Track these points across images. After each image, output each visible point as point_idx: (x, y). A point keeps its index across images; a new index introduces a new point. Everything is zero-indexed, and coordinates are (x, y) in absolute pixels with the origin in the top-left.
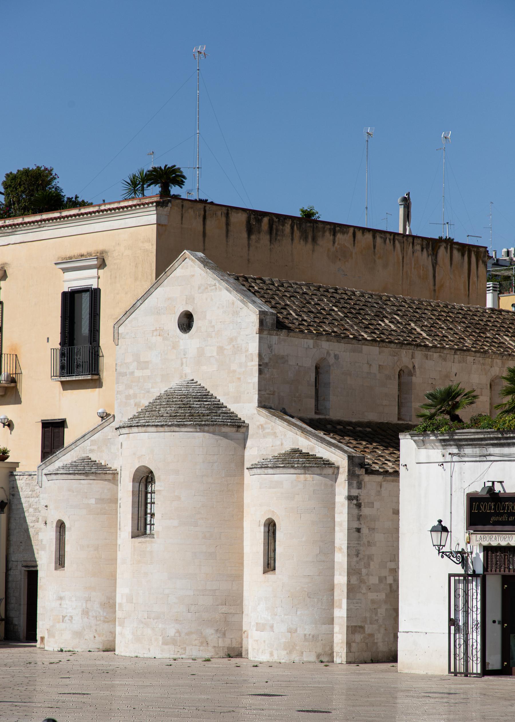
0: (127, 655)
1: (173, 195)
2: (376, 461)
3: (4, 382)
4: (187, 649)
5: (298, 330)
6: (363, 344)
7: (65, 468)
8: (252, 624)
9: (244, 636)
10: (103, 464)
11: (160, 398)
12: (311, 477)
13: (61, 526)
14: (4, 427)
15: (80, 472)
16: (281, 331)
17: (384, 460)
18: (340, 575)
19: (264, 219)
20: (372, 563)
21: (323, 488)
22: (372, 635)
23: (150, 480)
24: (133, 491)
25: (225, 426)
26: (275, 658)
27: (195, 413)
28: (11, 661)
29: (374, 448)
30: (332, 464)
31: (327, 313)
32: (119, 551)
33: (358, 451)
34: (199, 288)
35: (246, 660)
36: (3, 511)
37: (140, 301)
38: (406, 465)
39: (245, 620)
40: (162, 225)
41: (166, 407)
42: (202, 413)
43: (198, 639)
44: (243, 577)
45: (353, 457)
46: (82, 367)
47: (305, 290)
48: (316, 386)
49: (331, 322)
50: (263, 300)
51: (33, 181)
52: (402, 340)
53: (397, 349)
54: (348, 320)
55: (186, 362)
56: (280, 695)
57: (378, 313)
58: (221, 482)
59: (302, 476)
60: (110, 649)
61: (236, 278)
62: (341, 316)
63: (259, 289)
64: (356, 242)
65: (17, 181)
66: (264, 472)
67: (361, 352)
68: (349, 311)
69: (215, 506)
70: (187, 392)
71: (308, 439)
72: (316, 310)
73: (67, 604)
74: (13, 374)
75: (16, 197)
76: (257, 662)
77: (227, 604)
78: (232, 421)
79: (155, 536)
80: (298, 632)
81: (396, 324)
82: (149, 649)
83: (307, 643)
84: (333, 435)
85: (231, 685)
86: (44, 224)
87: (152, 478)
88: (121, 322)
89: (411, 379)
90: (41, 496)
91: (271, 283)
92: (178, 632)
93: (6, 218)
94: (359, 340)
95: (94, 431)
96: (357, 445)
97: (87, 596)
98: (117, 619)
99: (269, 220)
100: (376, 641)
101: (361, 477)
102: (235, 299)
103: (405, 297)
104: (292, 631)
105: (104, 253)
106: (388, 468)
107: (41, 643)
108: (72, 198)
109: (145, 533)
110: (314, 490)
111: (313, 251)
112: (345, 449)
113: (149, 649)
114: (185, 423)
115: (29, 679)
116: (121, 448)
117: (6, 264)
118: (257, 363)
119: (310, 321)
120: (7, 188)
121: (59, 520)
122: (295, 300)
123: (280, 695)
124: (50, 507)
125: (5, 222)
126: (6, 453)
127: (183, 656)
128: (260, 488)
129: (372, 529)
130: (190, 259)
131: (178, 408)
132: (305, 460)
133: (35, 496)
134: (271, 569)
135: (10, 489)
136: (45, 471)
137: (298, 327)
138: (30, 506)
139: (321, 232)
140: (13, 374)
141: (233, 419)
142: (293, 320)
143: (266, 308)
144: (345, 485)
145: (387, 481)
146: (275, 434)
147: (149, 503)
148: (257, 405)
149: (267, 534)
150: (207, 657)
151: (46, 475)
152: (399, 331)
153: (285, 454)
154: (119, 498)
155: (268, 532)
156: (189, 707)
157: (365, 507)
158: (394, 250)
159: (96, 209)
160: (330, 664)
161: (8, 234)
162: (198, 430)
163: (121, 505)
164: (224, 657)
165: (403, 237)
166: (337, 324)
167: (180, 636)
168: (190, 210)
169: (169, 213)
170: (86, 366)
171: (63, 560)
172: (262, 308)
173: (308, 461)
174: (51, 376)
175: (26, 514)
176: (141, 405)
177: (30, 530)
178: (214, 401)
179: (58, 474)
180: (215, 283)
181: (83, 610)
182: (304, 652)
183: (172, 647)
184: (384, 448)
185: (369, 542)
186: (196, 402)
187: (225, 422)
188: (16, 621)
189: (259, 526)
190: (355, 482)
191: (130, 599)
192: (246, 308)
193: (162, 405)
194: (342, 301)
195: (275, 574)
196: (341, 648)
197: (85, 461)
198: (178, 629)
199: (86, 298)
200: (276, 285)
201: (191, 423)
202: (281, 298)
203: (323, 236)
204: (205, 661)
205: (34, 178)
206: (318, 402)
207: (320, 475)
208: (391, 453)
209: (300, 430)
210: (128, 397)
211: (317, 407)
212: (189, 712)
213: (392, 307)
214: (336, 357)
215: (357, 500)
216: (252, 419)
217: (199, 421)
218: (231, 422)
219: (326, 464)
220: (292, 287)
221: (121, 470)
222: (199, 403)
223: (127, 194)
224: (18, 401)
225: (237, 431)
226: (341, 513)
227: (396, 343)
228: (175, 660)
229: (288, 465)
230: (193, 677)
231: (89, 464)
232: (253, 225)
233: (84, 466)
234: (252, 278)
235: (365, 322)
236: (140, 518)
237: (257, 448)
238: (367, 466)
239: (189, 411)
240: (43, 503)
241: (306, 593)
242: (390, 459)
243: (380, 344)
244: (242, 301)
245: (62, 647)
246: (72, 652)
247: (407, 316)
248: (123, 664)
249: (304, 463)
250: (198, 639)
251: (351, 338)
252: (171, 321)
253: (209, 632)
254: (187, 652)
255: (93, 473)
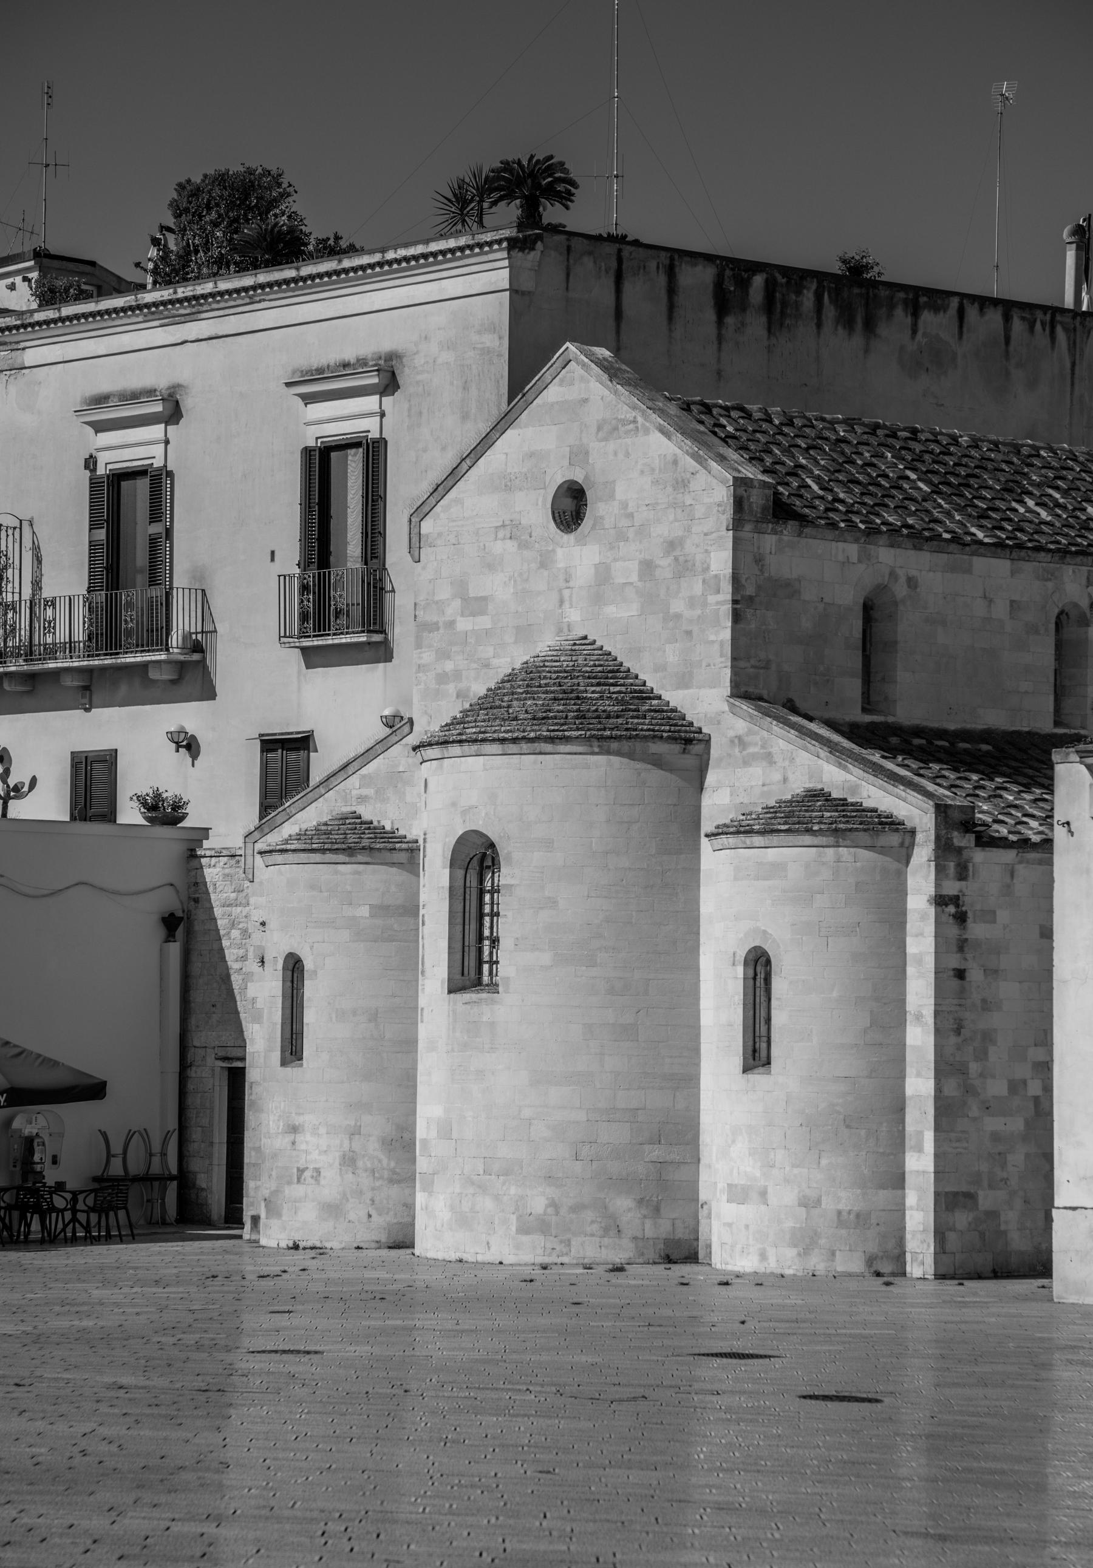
0: (440, 1256)
1: (549, 224)
2: (1001, 817)
3: (176, 650)
4: (573, 1243)
5: (823, 522)
6: (973, 554)
7: (302, 838)
8: (720, 1186)
9: (702, 1213)
10: (388, 828)
11: (511, 678)
12: (850, 853)
13: (294, 968)
14: (177, 751)
15: (336, 846)
16: (784, 523)
17: (1019, 815)
18: (919, 1075)
19: (754, 278)
20: (992, 1050)
21: (878, 878)
22: (993, 1215)
23: (488, 862)
24: (451, 888)
25: (656, 739)
26: (772, 1265)
27: (588, 711)
28: (175, 1271)
29: (998, 788)
30: (899, 824)
31: (893, 484)
32: (422, 1022)
33: (961, 796)
34: (599, 429)
35: (707, 1268)
36: (174, 936)
37: (468, 462)
38: (1068, 823)
39: (705, 1177)
40: (523, 293)
41: (525, 699)
42: (604, 711)
43: (599, 1220)
44: (699, 1079)
45: (947, 806)
46: (348, 616)
47: (842, 434)
48: (864, 650)
49: (900, 504)
50: (745, 456)
51: (237, 199)
52: (1065, 545)
53: (1051, 565)
54: (940, 501)
55: (571, 597)
56: (766, 1357)
57: (1011, 484)
58: (648, 865)
59: (830, 851)
60: (403, 1242)
61: (685, 407)
62: (925, 492)
63: (736, 430)
64: (965, 329)
65: (203, 200)
66: (745, 843)
67: (969, 571)
68: (943, 480)
69: (634, 921)
70: (571, 664)
71: (845, 768)
72: (867, 478)
73: (307, 1143)
74: (197, 633)
75: (199, 235)
76: (730, 1273)
77: (663, 1142)
78: (673, 728)
79: (501, 989)
80: (823, 1206)
81: (1052, 509)
82: (488, 1243)
83: (843, 1232)
84: (904, 759)
85: (658, 1329)
86: (260, 295)
87: (493, 859)
88: (426, 509)
89: (1086, 633)
90: (252, 900)
91: (764, 417)
92: (553, 1204)
93: (178, 282)
94: (965, 545)
95: (368, 755)
96: (958, 782)
97: (353, 1123)
98: (417, 1175)
99: (767, 281)
100: (1003, 1227)
101: (965, 853)
102: (678, 451)
103: (1074, 449)
104: (808, 1203)
105: (394, 358)
106: (1030, 832)
107: (252, 1228)
108: (328, 239)
109: (478, 982)
110: (857, 884)
111: (867, 351)
112: (929, 788)
113: (488, 1243)
114: (566, 733)
115: (196, 1316)
116: (425, 792)
117: (179, 386)
118: (729, 597)
119: (851, 501)
120: (180, 216)
121: (291, 953)
122: (818, 455)
123: (766, 1357)
124: (272, 925)
125: (175, 292)
126: (179, 807)
127: (565, 1260)
128: (736, 879)
129: (993, 972)
130: (578, 363)
131: (551, 699)
132: (837, 814)
133: (244, 901)
134: (761, 1063)
135: (189, 887)
136: (260, 846)
137: (825, 515)
138: (233, 925)
139: (884, 309)
140: (197, 633)
141: (676, 725)
142: (812, 499)
143: (750, 472)
144: (929, 872)
145: (1028, 862)
146: (769, 758)
147: (488, 915)
148: (728, 691)
149: (751, 982)
150: (618, 1260)
151: (260, 853)
152: (1058, 524)
153: (791, 802)
154: (421, 905)
155: (755, 979)
156: (542, 1386)
157: (975, 922)
158: (1053, 347)
159: (377, 257)
160: (896, 1280)
161: (183, 319)
162: (596, 750)
163: (426, 918)
164: (657, 1261)
165: (1074, 318)
166: (913, 509)
167: (557, 1213)
168: (586, 259)
169: (539, 266)
170: (357, 612)
171: (299, 1042)
172: (739, 472)
173: (844, 816)
174: (280, 637)
175: (225, 943)
176: (472, 694)
177: (233, 978)
178: (632, 685)
179: (286, 851)
180: (635, 417)
181: (344, 1156)
182: (838, 1253)
183: (538, 1239)
184: (1022, 788)
185: (984, 1001)
186: (592, 686)
187: (658, 731)
188: (202, 1181)
189: (734, 964)
190: (952, 864)
191: (445, 1131)
192: (704, 471)
193: (516, 693)
194: (927, 457)
195: (769, 1073)
196: (922, 1242)
197: (348, 821)
198: (553, 1199)
199: (355, 462)
200: (777, 422)
201: (580, 733)
202: (787, 451)
203: (890, 316)
204: (613, 1270)
205: (238, 191)
206: (869, 685)
207: (870, 848)
208: (1036, 800)
209: (825, 748)
210: (443, 678)
211: (868, 698)
212: (537, 1399)
213: (1043, 471)
214: (912, 583)
215: (957, 906)
216: (719, 723)
217: (599, 730)
218: (670, 731)
219: (886, 823)
220: (813, 426)
221: (425, 840)
222: (598, 689)
223: (447, 223)
224: (208, 693)
225: (684, 751)
226: (920, 934)
227: (1050, 550)
228: (545, 1268)
229: (797, 826)
230: (576, 1309)
231: (356, 829)
232: (730, 292)
233: (345, 834)
234: (721, 407)
235: (980, 504)
236: (466, 949)
237: (728, 789)
238: (979, 829)
239: (575, 707)
240: (257, 916)
241: (842, 1117)
242: (1035, 812)
243: (1014, 554)
244: (695, 457)
245: (296, 1239)
246: (318, 1251)
247: (1079, 490)
248: (425, 1277)
249: (836, 822)
250: (599, 1220)
251: (946, 540)
252: (537, 505)
253: (623, 1205)
254: (573, 1250)
255: (364, 848)
